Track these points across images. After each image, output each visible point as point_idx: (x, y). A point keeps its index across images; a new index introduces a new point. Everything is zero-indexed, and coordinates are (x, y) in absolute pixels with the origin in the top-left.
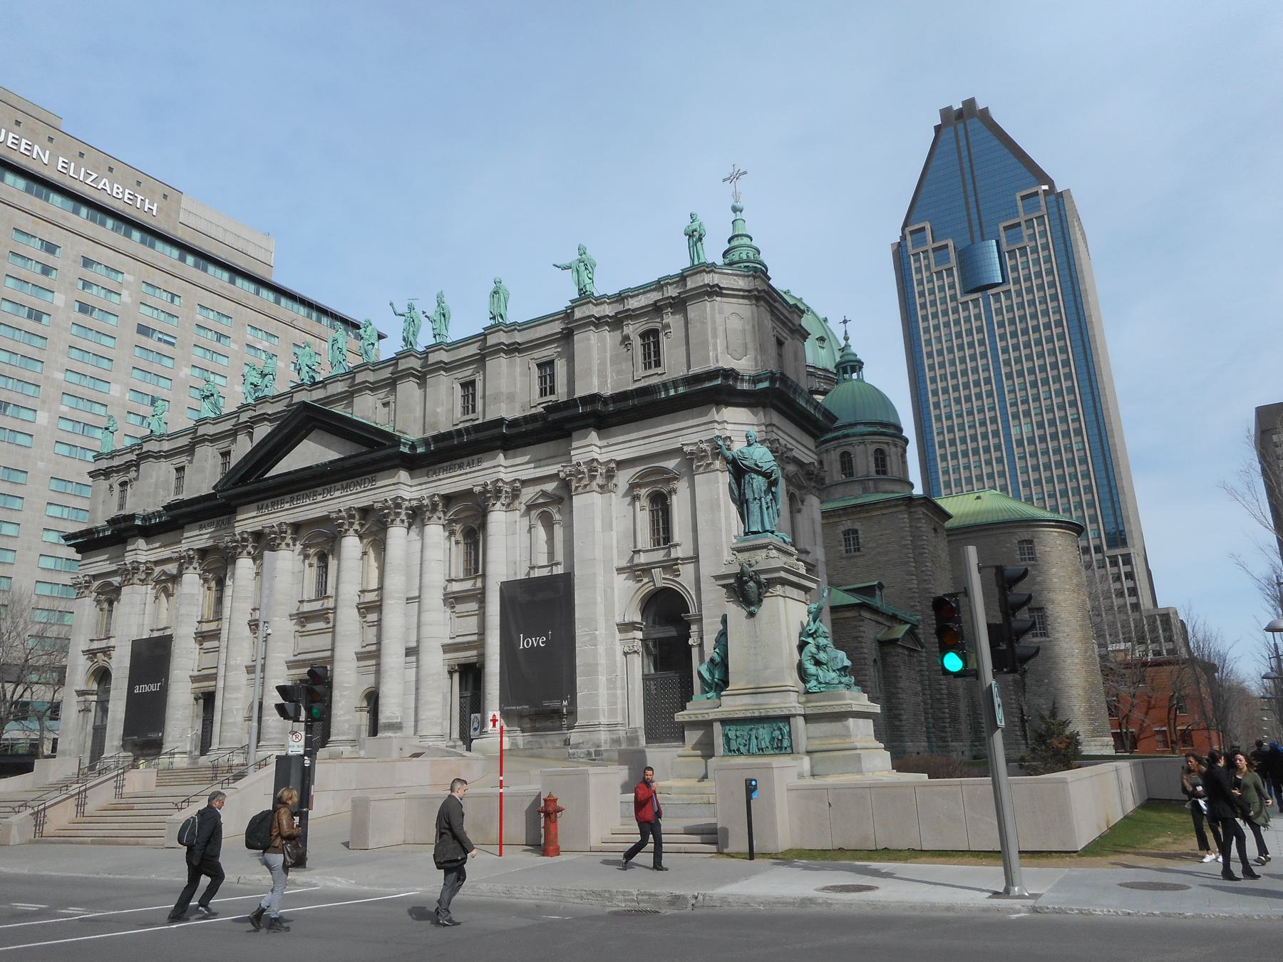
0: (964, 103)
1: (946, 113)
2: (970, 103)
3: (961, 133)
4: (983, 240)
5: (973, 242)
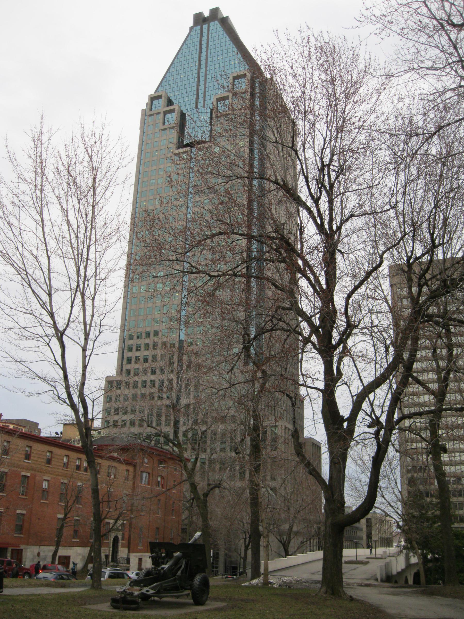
2: (215, 12)
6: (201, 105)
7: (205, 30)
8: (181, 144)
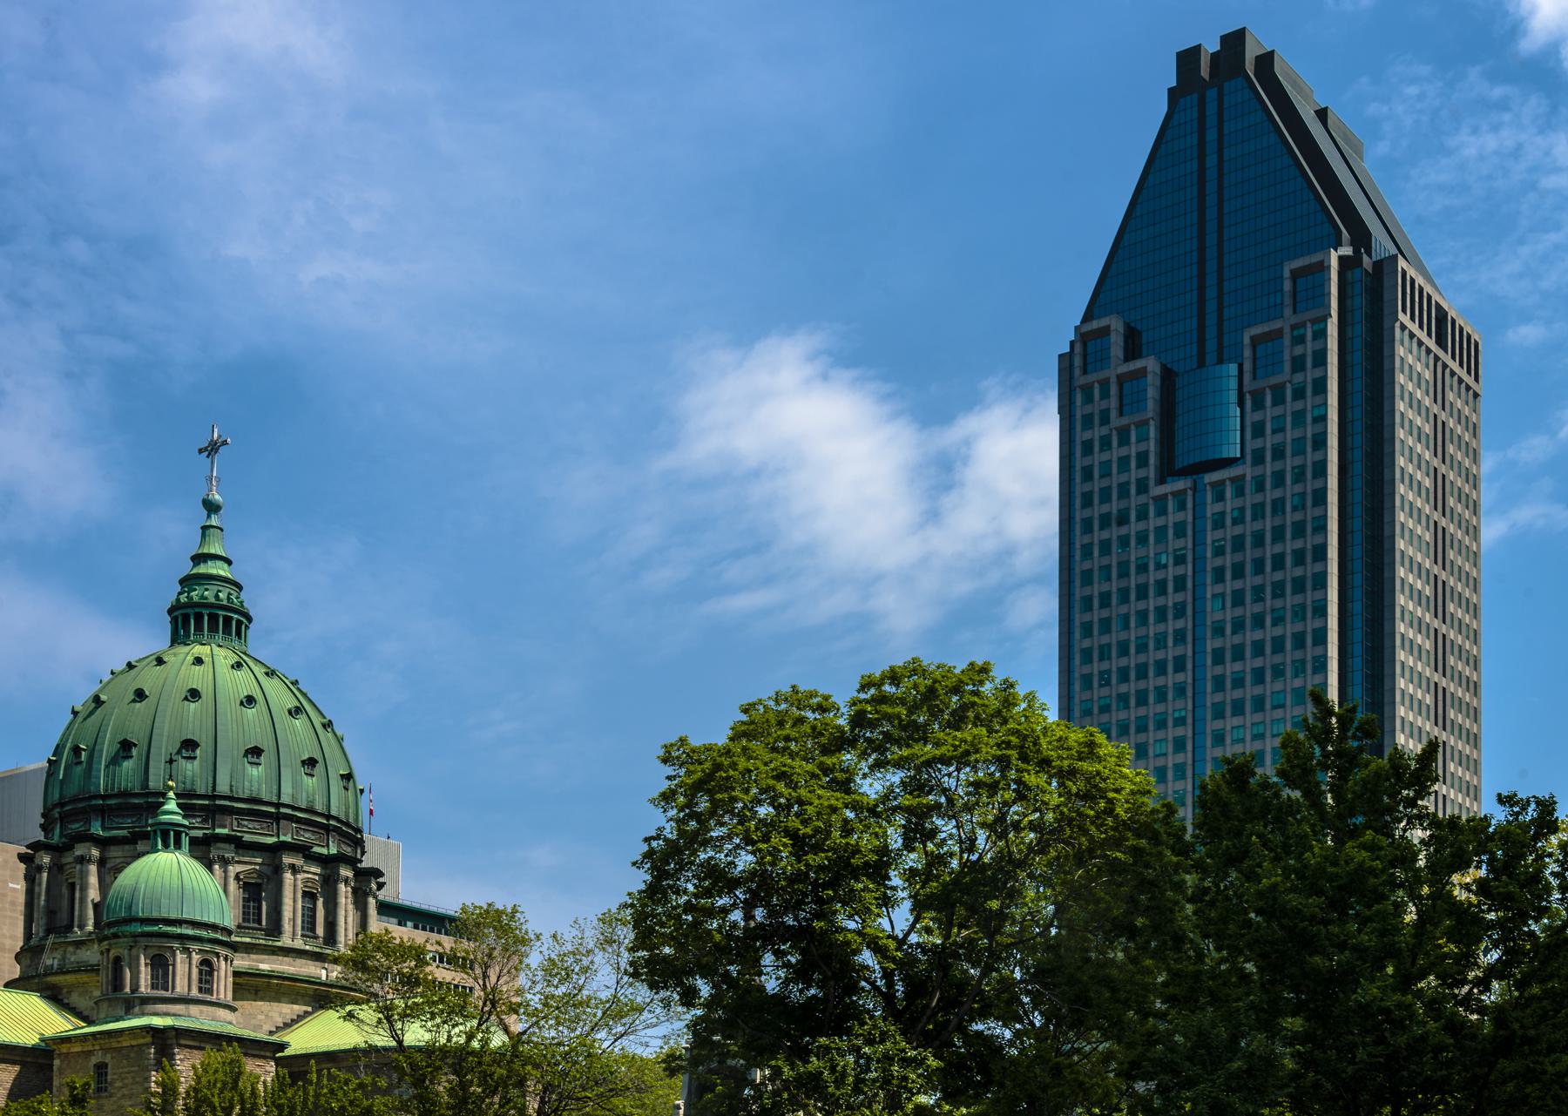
0: (1224, 39)
1: (1188, 59)
2: (1234, 41)
3: (1212, 109)
4: (1220, 361)
5: (1202, 363)
6: (1211, 345)
7: (1212, 109)
8: (1168, 470)
